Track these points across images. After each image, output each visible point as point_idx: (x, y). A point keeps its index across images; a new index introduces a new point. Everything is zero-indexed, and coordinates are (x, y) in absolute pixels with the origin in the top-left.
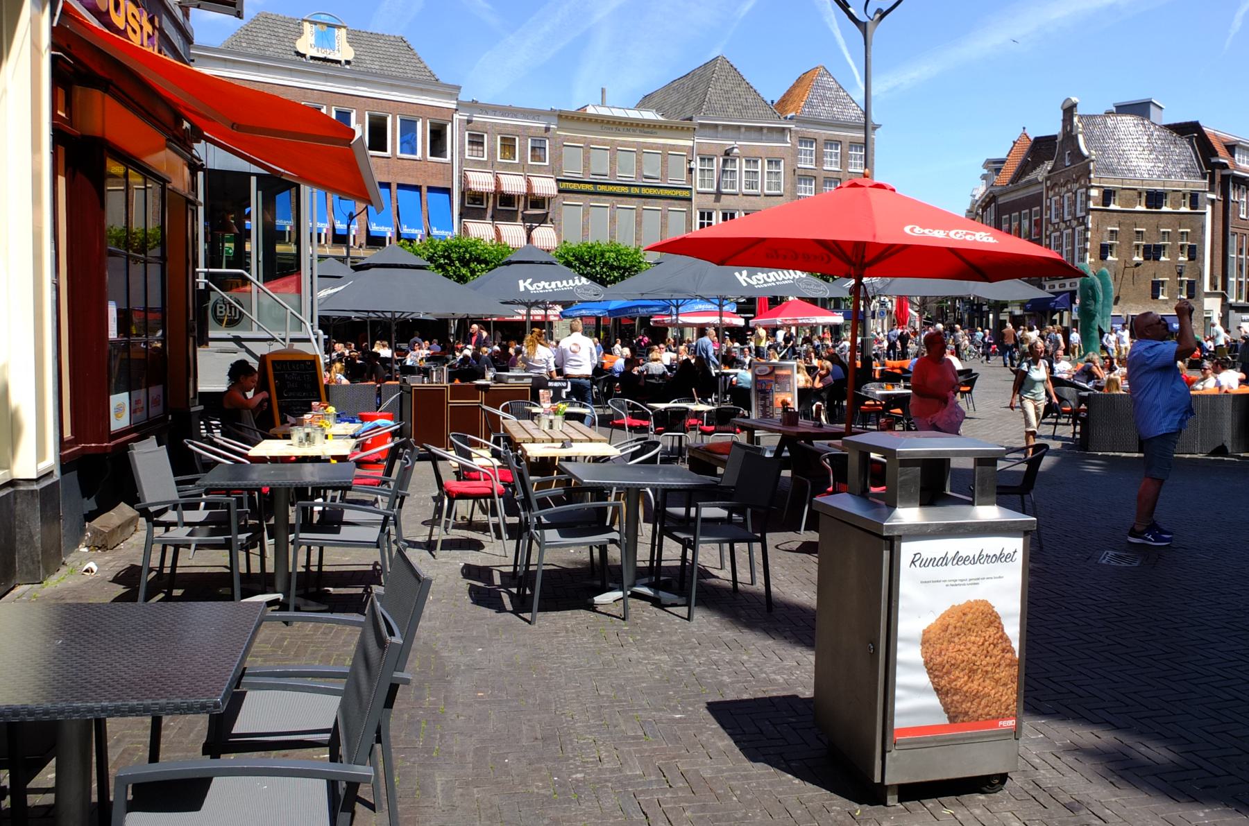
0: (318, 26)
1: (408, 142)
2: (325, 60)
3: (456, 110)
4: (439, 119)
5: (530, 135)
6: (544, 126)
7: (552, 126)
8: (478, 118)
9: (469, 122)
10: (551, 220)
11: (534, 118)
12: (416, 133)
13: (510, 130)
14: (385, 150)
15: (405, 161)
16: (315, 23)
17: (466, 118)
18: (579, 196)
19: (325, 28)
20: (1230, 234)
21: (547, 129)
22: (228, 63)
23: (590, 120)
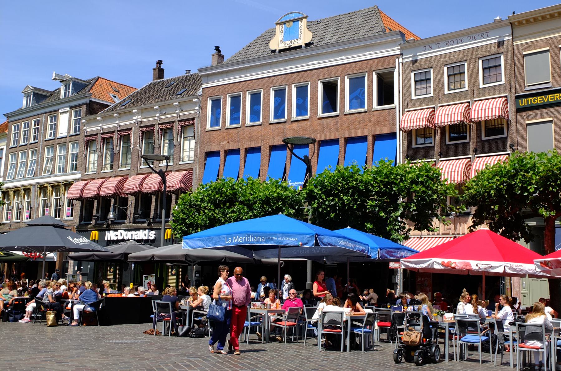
0: (287, 24)
1: (357, 98)
2: (290, 49)
3: (401, 54)
4: (383, 68)
5: (480, 56)
6: (496, 41)
7: (505, 39)
8: (422, 56)
9: (414, 62)
10: (512, 146)
11: (482, 37)
12: (364, 88)
13: (457, 58)
14: (380, 104)
15: (352, 116)
16: (284, 23)
17: (410, 59)
18: (547, 110)
19: (291, 23)
20: (508, 145)
21: (500, 44)
22: (209, 78)
23: (528, 21)
